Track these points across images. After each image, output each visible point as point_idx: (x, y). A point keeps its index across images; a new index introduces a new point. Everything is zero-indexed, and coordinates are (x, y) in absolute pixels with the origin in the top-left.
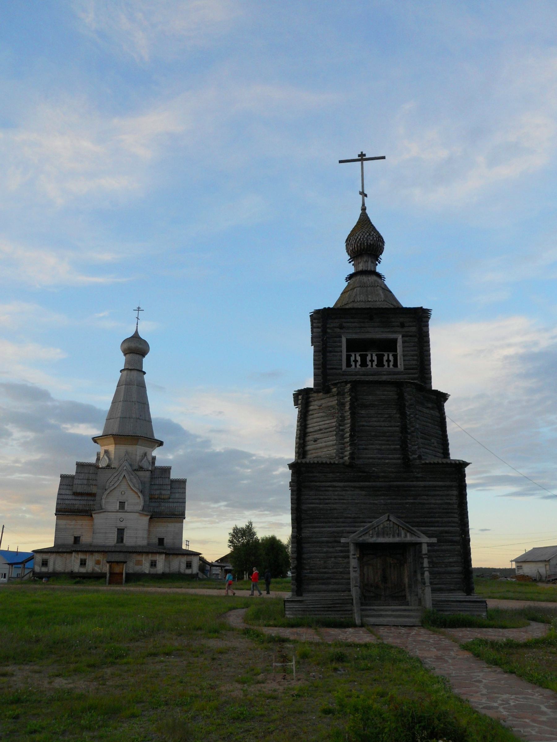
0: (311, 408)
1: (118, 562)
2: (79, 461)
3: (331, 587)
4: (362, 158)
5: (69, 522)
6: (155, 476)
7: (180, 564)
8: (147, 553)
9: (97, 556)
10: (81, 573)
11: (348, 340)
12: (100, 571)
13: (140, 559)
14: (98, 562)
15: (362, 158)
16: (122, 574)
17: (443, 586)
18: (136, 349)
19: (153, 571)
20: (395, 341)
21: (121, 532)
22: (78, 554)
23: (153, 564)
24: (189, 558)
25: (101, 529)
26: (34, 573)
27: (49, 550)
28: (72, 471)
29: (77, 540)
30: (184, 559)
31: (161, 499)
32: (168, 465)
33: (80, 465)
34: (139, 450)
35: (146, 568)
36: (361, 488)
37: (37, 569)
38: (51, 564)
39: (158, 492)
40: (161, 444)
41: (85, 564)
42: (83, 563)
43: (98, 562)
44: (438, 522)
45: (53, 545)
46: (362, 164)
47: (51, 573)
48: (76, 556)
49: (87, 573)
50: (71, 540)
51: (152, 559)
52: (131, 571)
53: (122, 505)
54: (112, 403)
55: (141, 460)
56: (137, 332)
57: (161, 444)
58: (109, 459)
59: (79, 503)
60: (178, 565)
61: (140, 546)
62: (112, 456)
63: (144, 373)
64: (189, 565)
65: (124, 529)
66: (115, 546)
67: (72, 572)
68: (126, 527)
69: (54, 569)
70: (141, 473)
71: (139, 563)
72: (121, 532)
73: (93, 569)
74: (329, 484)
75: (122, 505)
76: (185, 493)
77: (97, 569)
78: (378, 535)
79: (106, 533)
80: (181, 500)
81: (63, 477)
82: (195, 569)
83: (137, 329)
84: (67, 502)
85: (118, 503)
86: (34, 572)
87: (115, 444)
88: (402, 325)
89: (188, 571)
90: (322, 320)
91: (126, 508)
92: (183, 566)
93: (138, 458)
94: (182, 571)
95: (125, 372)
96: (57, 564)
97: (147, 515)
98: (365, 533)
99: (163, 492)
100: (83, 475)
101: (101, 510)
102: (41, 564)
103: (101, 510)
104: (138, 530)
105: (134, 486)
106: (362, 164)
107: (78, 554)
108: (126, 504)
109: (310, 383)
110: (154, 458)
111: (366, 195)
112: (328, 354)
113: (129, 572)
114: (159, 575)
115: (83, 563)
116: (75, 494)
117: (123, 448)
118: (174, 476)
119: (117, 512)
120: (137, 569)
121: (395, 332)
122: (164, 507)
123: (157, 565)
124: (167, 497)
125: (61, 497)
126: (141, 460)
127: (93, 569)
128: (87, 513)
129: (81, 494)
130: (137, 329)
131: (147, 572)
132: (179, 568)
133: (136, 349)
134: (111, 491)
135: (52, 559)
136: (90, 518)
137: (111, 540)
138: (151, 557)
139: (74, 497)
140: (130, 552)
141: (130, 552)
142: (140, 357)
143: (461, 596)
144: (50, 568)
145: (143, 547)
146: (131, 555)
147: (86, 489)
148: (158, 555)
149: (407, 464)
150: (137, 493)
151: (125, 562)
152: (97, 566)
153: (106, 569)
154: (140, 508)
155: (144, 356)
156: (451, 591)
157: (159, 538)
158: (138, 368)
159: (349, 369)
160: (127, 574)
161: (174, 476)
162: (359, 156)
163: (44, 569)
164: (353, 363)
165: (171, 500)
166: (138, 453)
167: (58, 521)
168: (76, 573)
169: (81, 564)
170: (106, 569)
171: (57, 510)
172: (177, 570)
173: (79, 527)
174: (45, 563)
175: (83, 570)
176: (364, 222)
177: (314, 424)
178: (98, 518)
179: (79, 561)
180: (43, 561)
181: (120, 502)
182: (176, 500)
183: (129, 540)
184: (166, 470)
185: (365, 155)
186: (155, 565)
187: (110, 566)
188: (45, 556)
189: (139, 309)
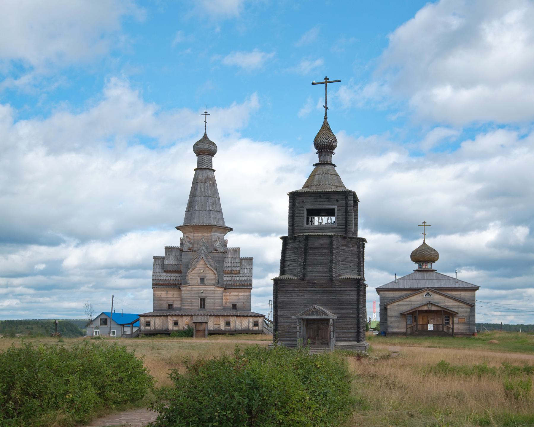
0: (288, 247)
2: (166, 245)
3: (292, 339)
4: (326, 81)
11: (307, 210)
15: (326, 81)
17: (347, 339)
20: (333, 209)
21: (203, 300)
24: (256, 319)
30: (251, 320)
33: (168, 249)
36: (309, 291)
37: (143, 328)
38: (152, 323)
40: (231, 230)
41: (177, 324)
42: (176, 324)
44: (346, 308)
46: (326, 86)
50: (165, 307)
53: (202, 280)
54: (193, 184)
56: (205, 134)
57: (231, 230)
60: (246, 323)
63: (214, 171)
72: (203, 300)
74: (291, 289)
75: (202, 280)
78: (309, 315)
79: (191, 301)
83: (205, 133)
85: (199, 279)
88: (337, 201)
90: (294, 196)
92: (251, 325)
95: (199, 171)
98: (303, 314)
101: (186, 283)
103: (186, 283)
105: (211, 266)
106: (326, 86)
108: (205, 279)
109: (287, 235)
110: (226, 242)
111: (328, 108)
112: (296, 218)
118: (242, 255)
121: (334, 204)
128: (177, 286)
130: (205, 133)
135: (152, 320)
136: (178, 290)
139: (165, 274)
142: (210, 157)
143: (354, 343)
149: (331, 279)
151: (206, 323)
155: (213, 156)
156: (350, 341)
158: (208, 167)
159: (308, 226)
162: (324, 79)
163: (148, 328)
164: (310, 223)
165: (241, 275)
171: (153, 284)
174: (148, 324)
176: (325, 128)
177: (290, 256)
184: (237, 250)
185: (328, 79)
188: (148, 319)
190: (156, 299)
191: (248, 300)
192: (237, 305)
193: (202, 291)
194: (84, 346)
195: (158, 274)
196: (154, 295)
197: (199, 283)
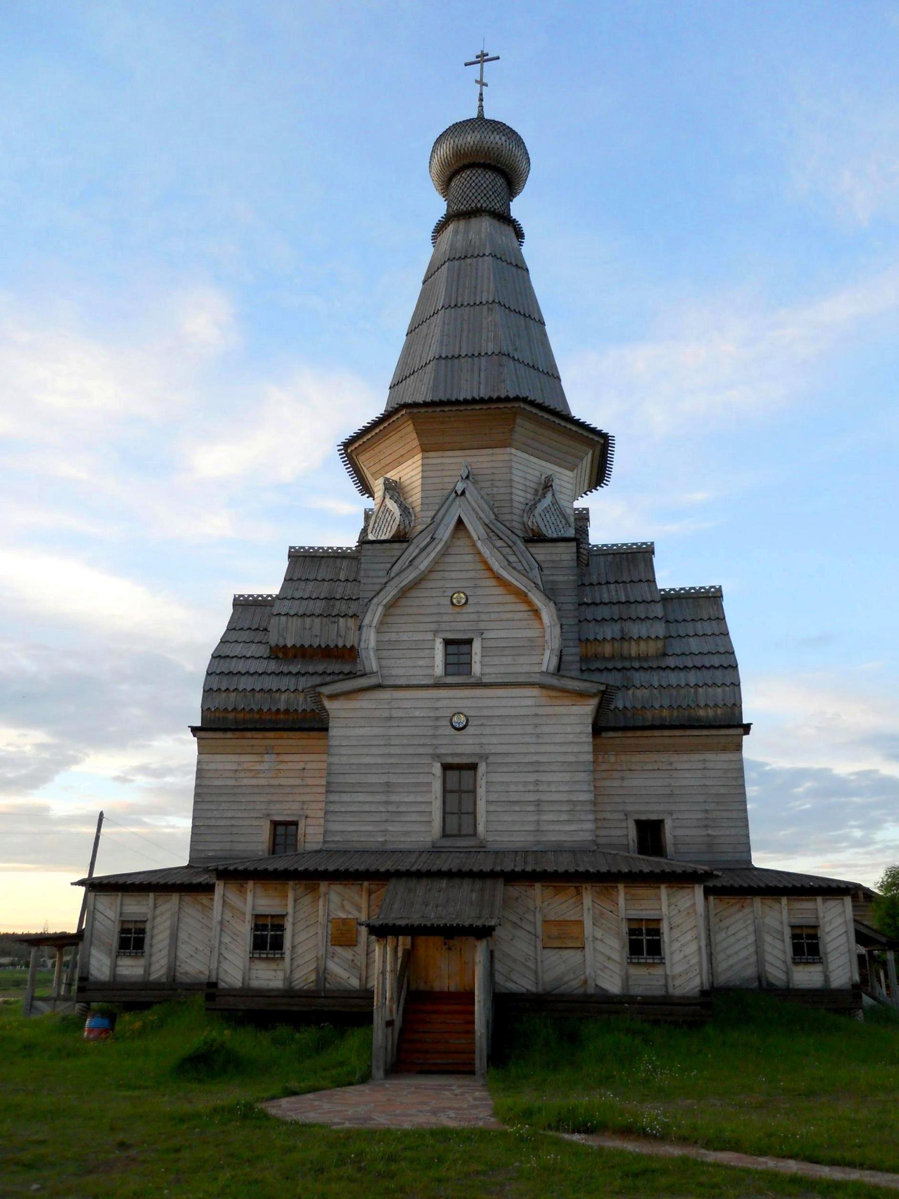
1: (450, 933)
2: (298, 544)
5: (248, 760)
6: (594, 579)
7: (759, 944)
8: (605, 880)
9: (345, 904)
10: (261, 993)
12: (355, 983)
13: (571, 916)
14: (343, 936)
16: (469, 996)
18: (482, 171)
19: (646, 980)
21: (459, 772)
22: (242, 891)
23: (645, 942)
24: (805, 910)
25: (372, 778)
26: (86, 986)
27: (154, 880)
28: (269, 582)
29: (284, 831)
30: (779, 916)
31: (630, 658)
32: (639, 539)
33: (303, 561)
34: (519, 467)
35: (603, 964)
39: (610, 631)
41: (277, 944)
42: (268, 938)
43: (343, 936)
45: (185, 862)
47: (157, 986)
48: (233, 898)
49: (289, 993)
51: (634, 914)
52: (523, 983)
53: (458, 648)
55: (531, 508)
58: (405, 510)
59: (289, 691)
61: (559, 850)
62: (415, 498)
64: (806, 945)
65: (473, 767)
66: (435, 851)
67: (214, 985)
68: (485, 757)
69: (172, 968)
70: (541, 552)
71: (565, 936)
72: (459, 772)
73: (322, 974)
75: (458, 648)
76: (726, 634)
77: (343, 972)
80: (716, 661)
81: (242, 604)
82: (840, 965)
83: (481, 106)
84: (245, 683)
85: (439, 646)
86: (84, 979)
87: (423, 451)
89: (807, 977)
91: (476, 669)
93: (520, 497)
94: (776, 973)
96: (212, 945)
97: (582, 695)
99: (636, 630)
100: (310, 585)
102: (115, 942)
104: (543, 775)
107: (242, 891)
108: (477, 646)
110: (583, 517)
113: (512, 987)
114: (684, 1002)
115: (268, 938)
116: (280, 653)
117: (454, 464)
118: (669, 576)
119: (437, 686)
120: (559, 969)
122: (642, 693)
123: (666, 949)
124: (652, 648)
125: (225, 666)
126: (531, 508)
127: (322, 974)
129: (301, 653)
131: (613, 986)
132: (760, 962)
133: (482, 171)
134: (404, 592)
137: (415, 821)
138: (625, 904)
139: (273, 666)
140: (512, 878)
141: (512, 878)
144: (155, 964)
145: (575, 851)
146: (515, 891)
147: (317, 633)
148: (664, 891)
150: (523, 597)
151: (484, 932)
152: (345, 953)
153: (375, 969)
154: (548, 660)
157: (639, 823)
160: (505, 1004)
161: (669, 576)
163: (131, 968)
166: (517, 477)
167: (206, 757)
168: (232, 993)
169: (259, 944)
170: (375, 969)
172: (751, 972)
173: (284, 779)
174: (132, 940)
175: (268, 976)
178: (353, 721)
179: (245, 930)
180: (123, 931)
181: (448, 643)
182: (698, 661)
183: (505, 821)
184: (638, 557)
186: (655, 949)
187: (409, 963)
188: (136, 907)
189: (483, 58)
190: (205, 795)
191: (730, 798)
192: (669, 833)
193: (460, 720)
194: (467, 1095)
195: (240, 666)
196: (200, 773)
197: (439, 670)
